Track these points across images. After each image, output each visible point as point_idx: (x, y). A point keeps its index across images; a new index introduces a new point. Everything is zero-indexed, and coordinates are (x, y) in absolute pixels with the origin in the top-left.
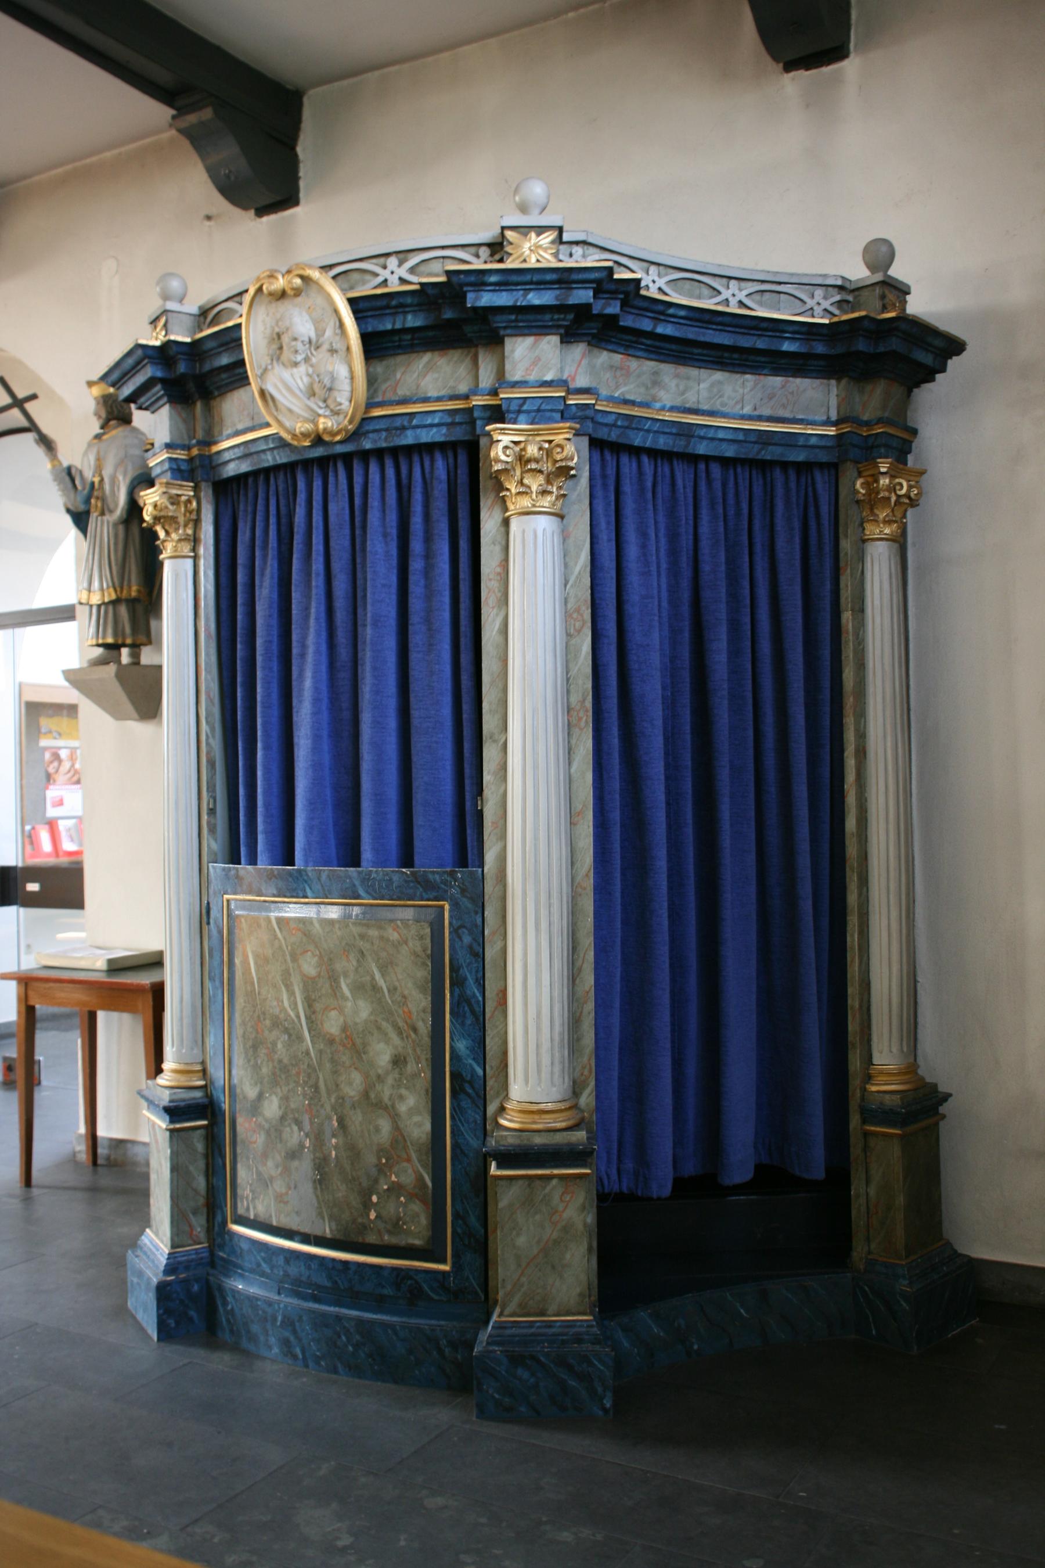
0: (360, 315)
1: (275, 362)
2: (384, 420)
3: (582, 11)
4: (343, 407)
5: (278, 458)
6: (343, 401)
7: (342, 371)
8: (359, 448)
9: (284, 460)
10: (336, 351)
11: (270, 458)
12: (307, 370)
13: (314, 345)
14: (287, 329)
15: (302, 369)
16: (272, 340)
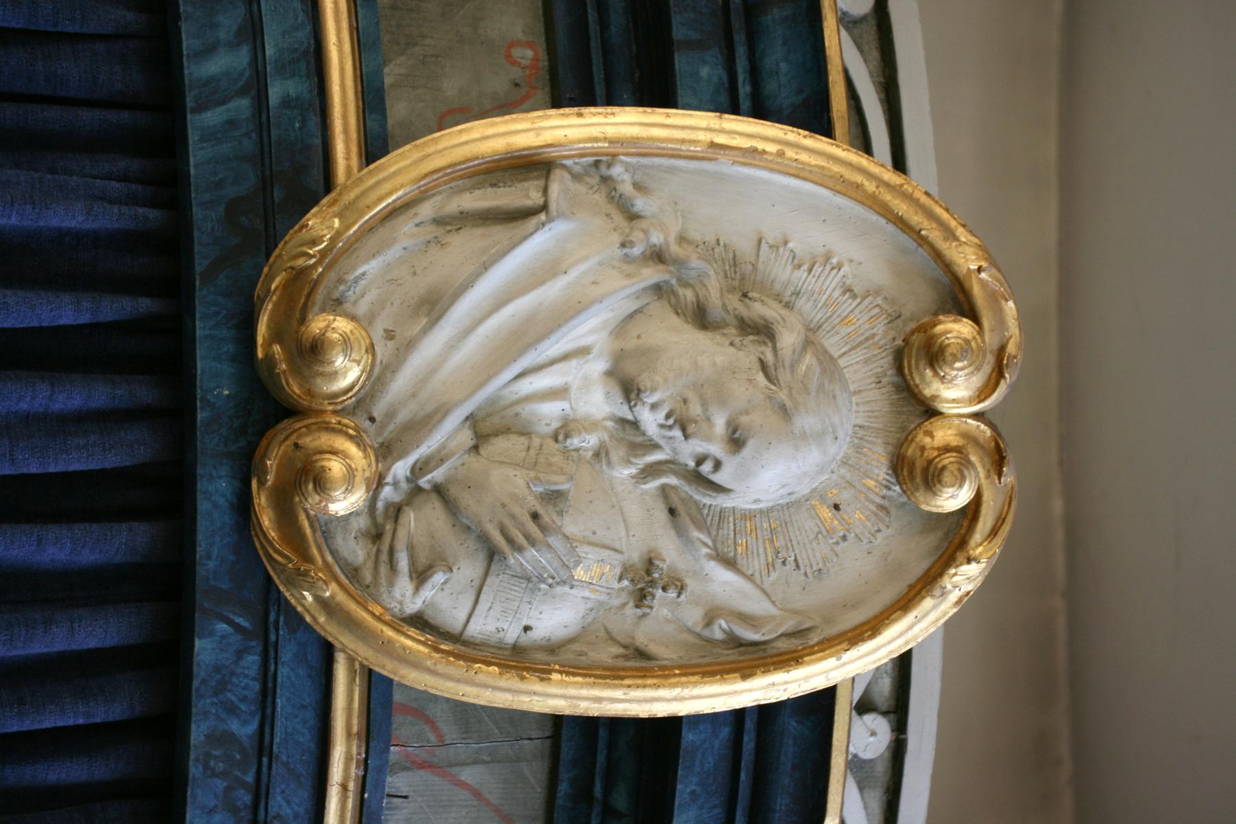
0: (749, 725)
1: (652, 275)
2: (306, 738)
3: (1059, 535)
4: (404, 585)
5: (213, 117)
6: (427, 593)
7: (553, 619)
8: (203, 602)
9: (198, 154)
10: (641, 597)
11: (214, 66)
12: (593, 426)
13: (689, 495)
14: (785, 412)
15: (599, 403)
16: (743, 283)
